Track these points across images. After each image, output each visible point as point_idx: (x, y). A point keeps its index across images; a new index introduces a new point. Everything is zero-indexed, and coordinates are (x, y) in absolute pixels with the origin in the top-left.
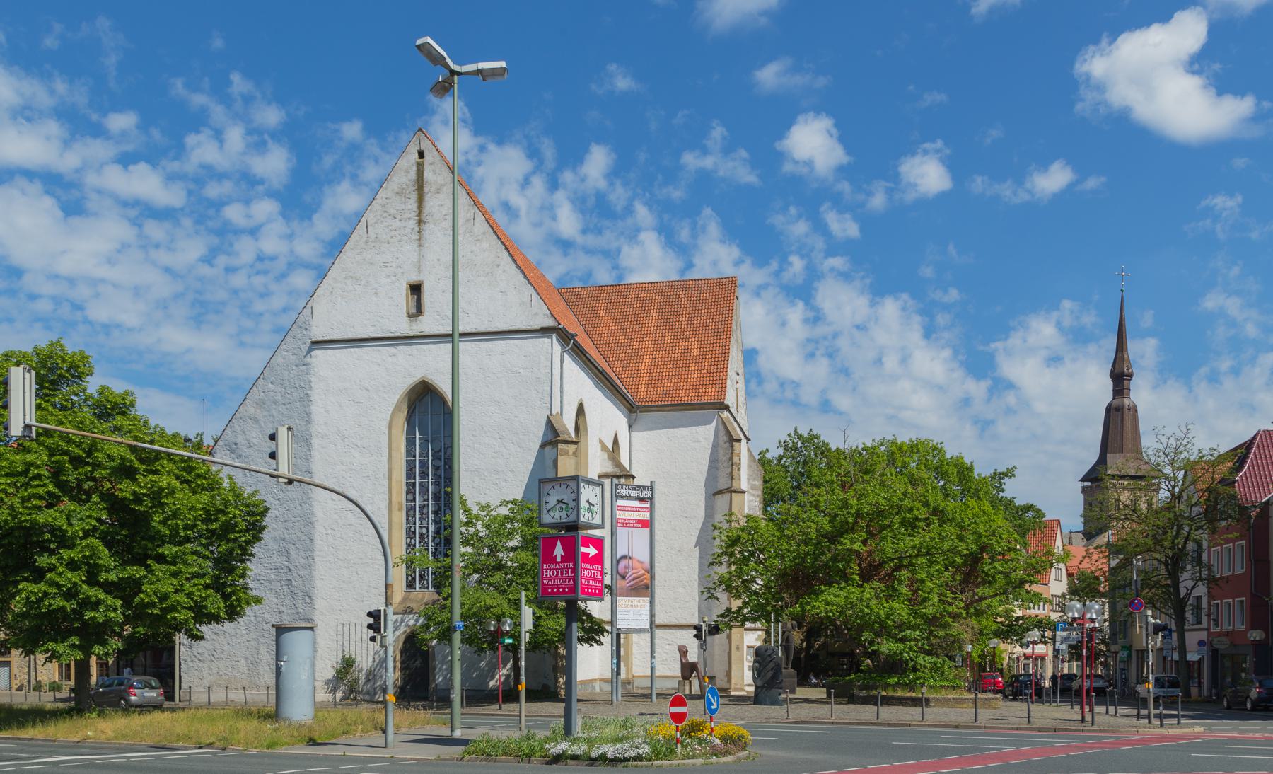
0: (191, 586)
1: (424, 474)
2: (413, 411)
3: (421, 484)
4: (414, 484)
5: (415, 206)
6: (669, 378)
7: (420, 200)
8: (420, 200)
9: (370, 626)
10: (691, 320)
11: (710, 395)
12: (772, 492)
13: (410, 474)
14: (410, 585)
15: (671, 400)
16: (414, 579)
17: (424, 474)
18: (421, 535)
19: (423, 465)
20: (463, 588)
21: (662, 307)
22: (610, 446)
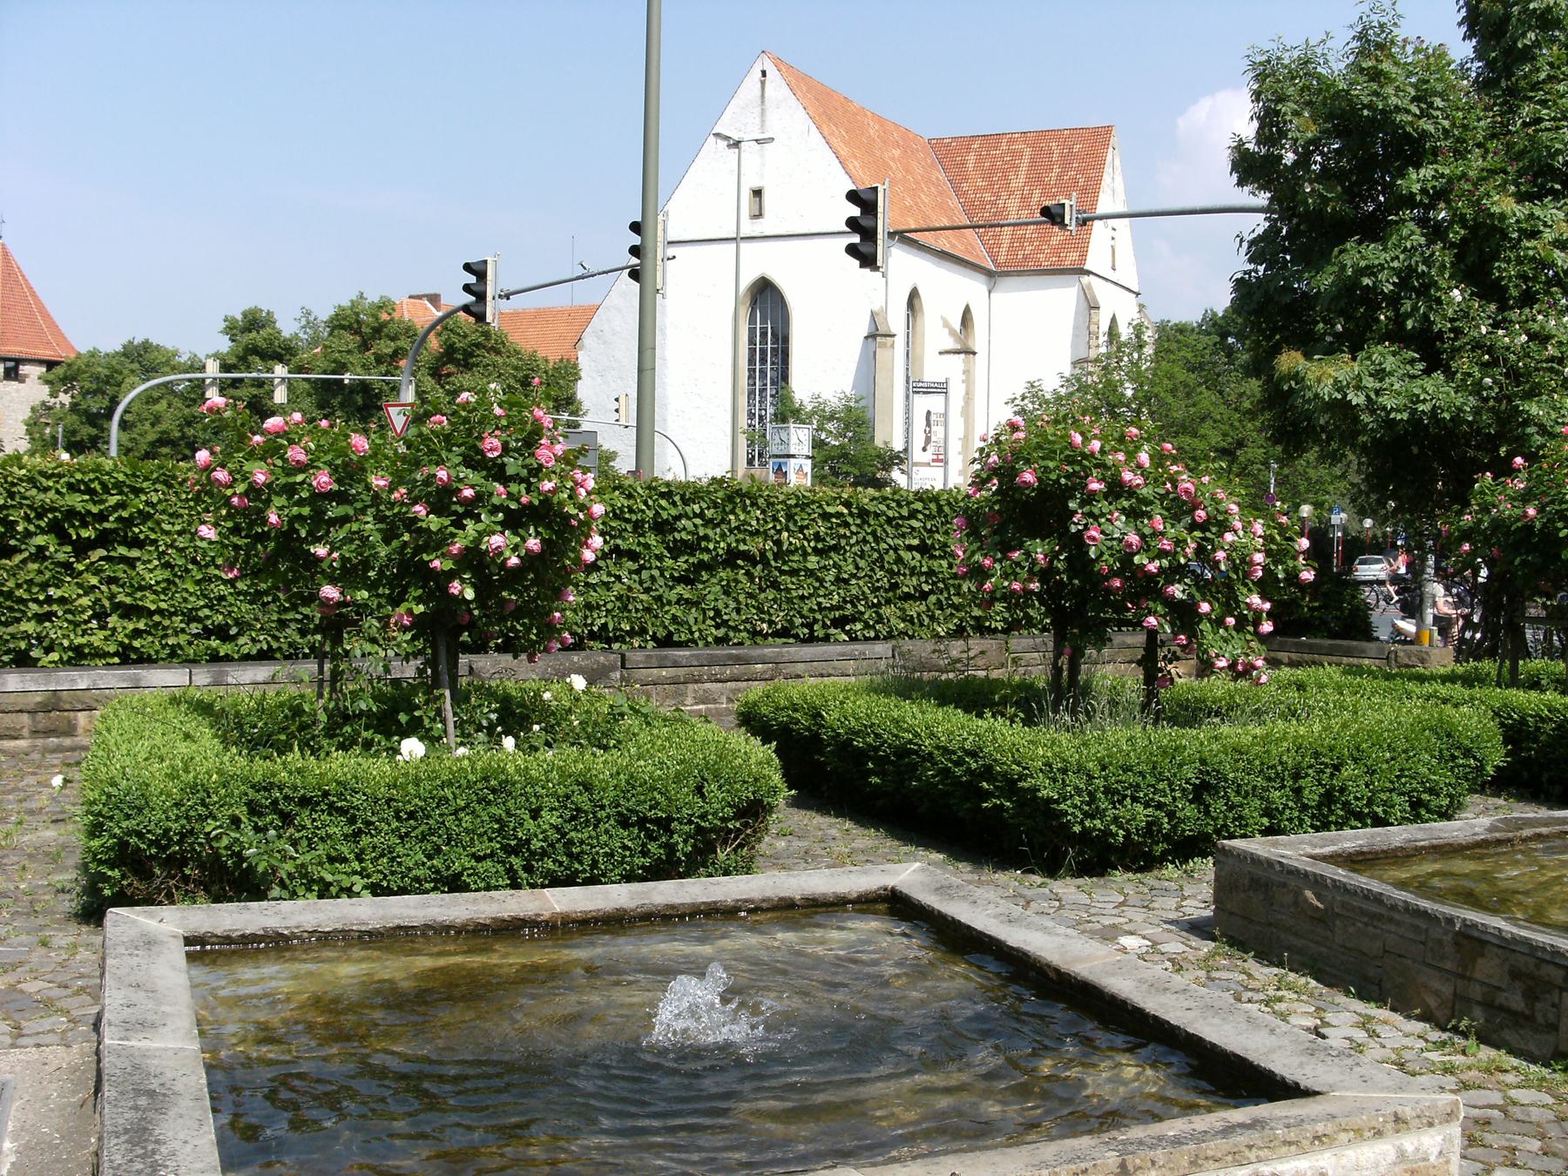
0: (419, 450)
1: (763, 361)
2: (755, 303)
3: (761, 370)
4: (754, 370)
5: (758, 121)
6: (1031, 242)
7: (763, 112)
8: (763, 112)
9: (467, 288)
10: (1059, 176)
11: (1071, 258)
12: (582, 800)
13: (751, 361)
14: (750, 462)
15: (1031, 265)
16: (753, 457)
17: (763, 361)
18: (760, 416)
19: (764, 352)
20: (846, 1072)
21: (1032, 161)
22: (957, 326)
